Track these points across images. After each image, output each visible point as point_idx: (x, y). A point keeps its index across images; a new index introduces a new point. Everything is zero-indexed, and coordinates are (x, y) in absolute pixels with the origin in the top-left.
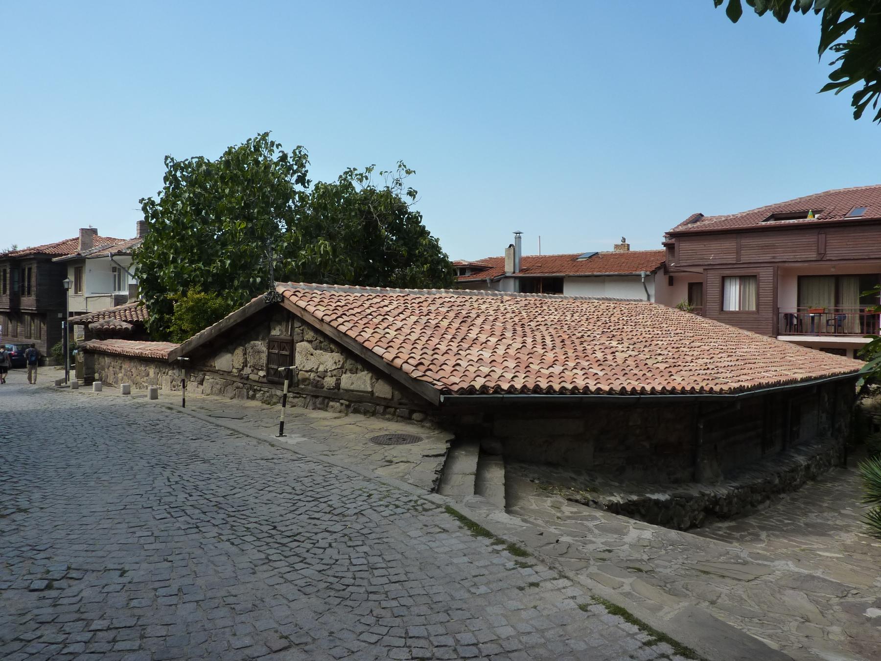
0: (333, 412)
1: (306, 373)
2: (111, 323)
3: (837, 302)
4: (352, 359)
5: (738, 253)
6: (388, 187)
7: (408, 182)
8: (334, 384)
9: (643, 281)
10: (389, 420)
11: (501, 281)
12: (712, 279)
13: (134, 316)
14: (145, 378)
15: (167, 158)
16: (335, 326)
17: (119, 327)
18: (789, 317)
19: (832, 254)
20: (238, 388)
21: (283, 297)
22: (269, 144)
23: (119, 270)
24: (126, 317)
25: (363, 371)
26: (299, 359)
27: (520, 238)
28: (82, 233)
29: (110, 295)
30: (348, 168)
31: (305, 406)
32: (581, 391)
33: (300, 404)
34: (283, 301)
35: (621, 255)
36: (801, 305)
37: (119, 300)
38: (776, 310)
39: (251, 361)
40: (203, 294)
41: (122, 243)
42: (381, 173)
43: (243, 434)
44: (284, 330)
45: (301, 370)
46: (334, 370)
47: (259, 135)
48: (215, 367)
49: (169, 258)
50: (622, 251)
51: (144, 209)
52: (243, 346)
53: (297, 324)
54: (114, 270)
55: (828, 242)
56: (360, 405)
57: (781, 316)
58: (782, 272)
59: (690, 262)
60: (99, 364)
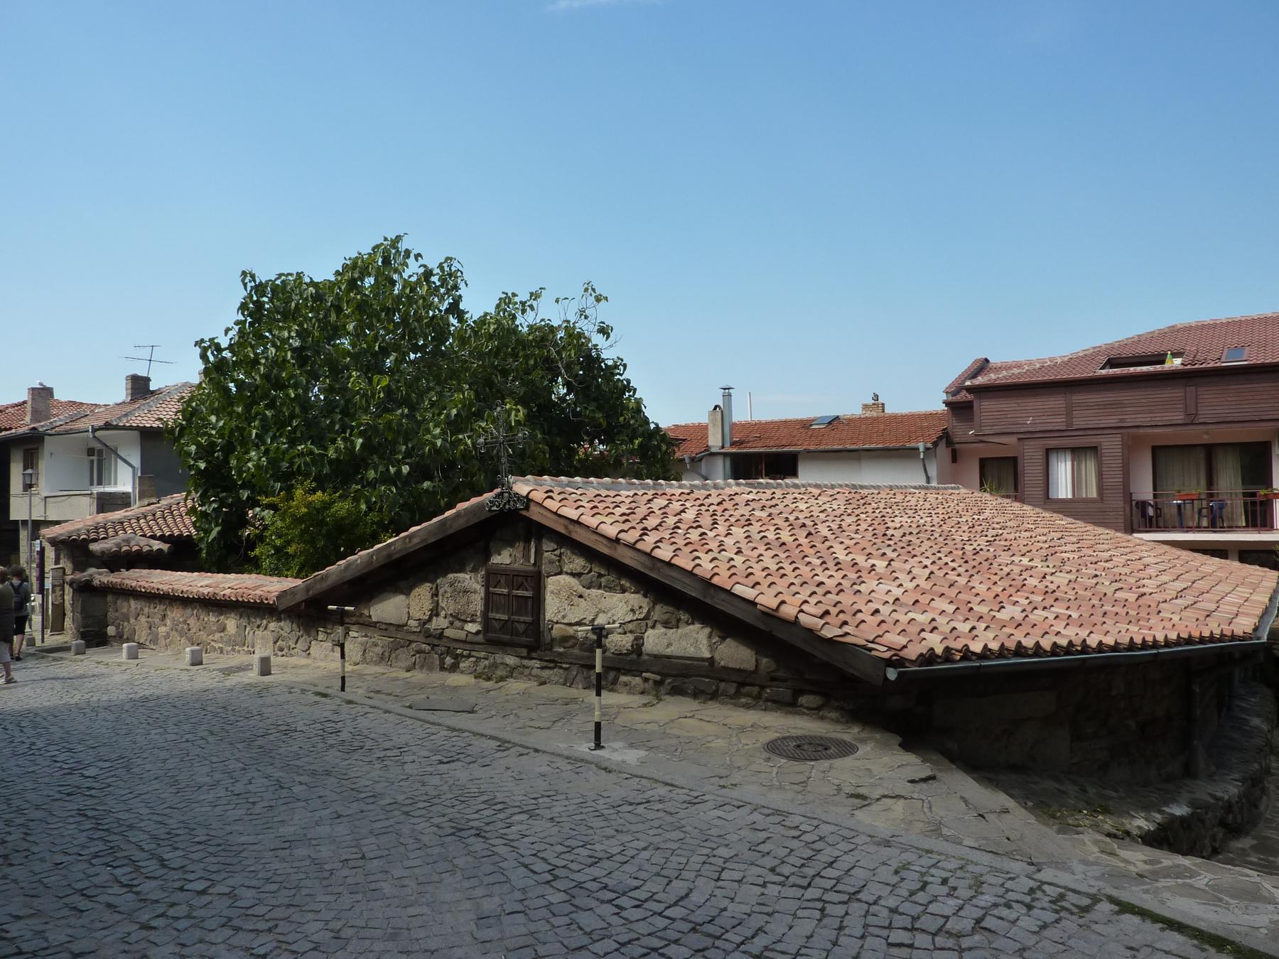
0: (629, 693)
1: (568, 628)
2: (133, 543)
3: (1210, 483)
4: (667, 604)
5: (1069, 414)
6: (568, 322)
7: (602, 313)
8: (629, 646)
9: (922, 457)
10: (747, 707)
11: (703, 462)
12: (1031, 456)
13: (155, 528)
14: (217, 636)
15: (244, 273)
16: (648, 550)
17: (146, 549)
18: (1143, 505)
19: (1206, 413)
20: (419, 652)
21: (528, 501)
22: (402, 254)
23: (100, 452)
24: (141, 529)
25: (693, 623)
26: (553, 607)
27: (730, 395)
28: (33, 394)
29: (89, 492)
30: (503, 293)
31: (568, 682)
32: (1079, 648)
33: (555, 679)
34: (527, 508)
35: (876, 420)
36: (1158, 489)
37: (106, 503)
38: (1128, 496)
39: (448, 605)
40: (319, 493)
41: (102, 410)
42: (557, 301)
43: (470, 732)
44: (519, 555)
45: (557, 623)
46: (629, 622)
47: (386, 239)
48: (370, 617)
49: (251, 435)
50: (874, 414)
51: (204, 357)
52: (432, 581)
53: (548, 545)
54: (91, 452)
55: (1200, 397)
56: (686, 680)
57: (1134, 503)
58: (1132, 443)
59: (997, 429)
60: (117, 611)
